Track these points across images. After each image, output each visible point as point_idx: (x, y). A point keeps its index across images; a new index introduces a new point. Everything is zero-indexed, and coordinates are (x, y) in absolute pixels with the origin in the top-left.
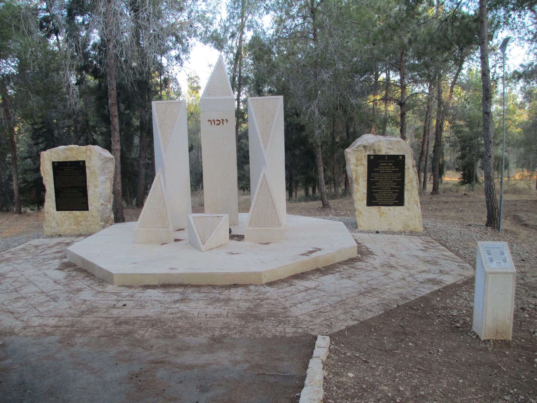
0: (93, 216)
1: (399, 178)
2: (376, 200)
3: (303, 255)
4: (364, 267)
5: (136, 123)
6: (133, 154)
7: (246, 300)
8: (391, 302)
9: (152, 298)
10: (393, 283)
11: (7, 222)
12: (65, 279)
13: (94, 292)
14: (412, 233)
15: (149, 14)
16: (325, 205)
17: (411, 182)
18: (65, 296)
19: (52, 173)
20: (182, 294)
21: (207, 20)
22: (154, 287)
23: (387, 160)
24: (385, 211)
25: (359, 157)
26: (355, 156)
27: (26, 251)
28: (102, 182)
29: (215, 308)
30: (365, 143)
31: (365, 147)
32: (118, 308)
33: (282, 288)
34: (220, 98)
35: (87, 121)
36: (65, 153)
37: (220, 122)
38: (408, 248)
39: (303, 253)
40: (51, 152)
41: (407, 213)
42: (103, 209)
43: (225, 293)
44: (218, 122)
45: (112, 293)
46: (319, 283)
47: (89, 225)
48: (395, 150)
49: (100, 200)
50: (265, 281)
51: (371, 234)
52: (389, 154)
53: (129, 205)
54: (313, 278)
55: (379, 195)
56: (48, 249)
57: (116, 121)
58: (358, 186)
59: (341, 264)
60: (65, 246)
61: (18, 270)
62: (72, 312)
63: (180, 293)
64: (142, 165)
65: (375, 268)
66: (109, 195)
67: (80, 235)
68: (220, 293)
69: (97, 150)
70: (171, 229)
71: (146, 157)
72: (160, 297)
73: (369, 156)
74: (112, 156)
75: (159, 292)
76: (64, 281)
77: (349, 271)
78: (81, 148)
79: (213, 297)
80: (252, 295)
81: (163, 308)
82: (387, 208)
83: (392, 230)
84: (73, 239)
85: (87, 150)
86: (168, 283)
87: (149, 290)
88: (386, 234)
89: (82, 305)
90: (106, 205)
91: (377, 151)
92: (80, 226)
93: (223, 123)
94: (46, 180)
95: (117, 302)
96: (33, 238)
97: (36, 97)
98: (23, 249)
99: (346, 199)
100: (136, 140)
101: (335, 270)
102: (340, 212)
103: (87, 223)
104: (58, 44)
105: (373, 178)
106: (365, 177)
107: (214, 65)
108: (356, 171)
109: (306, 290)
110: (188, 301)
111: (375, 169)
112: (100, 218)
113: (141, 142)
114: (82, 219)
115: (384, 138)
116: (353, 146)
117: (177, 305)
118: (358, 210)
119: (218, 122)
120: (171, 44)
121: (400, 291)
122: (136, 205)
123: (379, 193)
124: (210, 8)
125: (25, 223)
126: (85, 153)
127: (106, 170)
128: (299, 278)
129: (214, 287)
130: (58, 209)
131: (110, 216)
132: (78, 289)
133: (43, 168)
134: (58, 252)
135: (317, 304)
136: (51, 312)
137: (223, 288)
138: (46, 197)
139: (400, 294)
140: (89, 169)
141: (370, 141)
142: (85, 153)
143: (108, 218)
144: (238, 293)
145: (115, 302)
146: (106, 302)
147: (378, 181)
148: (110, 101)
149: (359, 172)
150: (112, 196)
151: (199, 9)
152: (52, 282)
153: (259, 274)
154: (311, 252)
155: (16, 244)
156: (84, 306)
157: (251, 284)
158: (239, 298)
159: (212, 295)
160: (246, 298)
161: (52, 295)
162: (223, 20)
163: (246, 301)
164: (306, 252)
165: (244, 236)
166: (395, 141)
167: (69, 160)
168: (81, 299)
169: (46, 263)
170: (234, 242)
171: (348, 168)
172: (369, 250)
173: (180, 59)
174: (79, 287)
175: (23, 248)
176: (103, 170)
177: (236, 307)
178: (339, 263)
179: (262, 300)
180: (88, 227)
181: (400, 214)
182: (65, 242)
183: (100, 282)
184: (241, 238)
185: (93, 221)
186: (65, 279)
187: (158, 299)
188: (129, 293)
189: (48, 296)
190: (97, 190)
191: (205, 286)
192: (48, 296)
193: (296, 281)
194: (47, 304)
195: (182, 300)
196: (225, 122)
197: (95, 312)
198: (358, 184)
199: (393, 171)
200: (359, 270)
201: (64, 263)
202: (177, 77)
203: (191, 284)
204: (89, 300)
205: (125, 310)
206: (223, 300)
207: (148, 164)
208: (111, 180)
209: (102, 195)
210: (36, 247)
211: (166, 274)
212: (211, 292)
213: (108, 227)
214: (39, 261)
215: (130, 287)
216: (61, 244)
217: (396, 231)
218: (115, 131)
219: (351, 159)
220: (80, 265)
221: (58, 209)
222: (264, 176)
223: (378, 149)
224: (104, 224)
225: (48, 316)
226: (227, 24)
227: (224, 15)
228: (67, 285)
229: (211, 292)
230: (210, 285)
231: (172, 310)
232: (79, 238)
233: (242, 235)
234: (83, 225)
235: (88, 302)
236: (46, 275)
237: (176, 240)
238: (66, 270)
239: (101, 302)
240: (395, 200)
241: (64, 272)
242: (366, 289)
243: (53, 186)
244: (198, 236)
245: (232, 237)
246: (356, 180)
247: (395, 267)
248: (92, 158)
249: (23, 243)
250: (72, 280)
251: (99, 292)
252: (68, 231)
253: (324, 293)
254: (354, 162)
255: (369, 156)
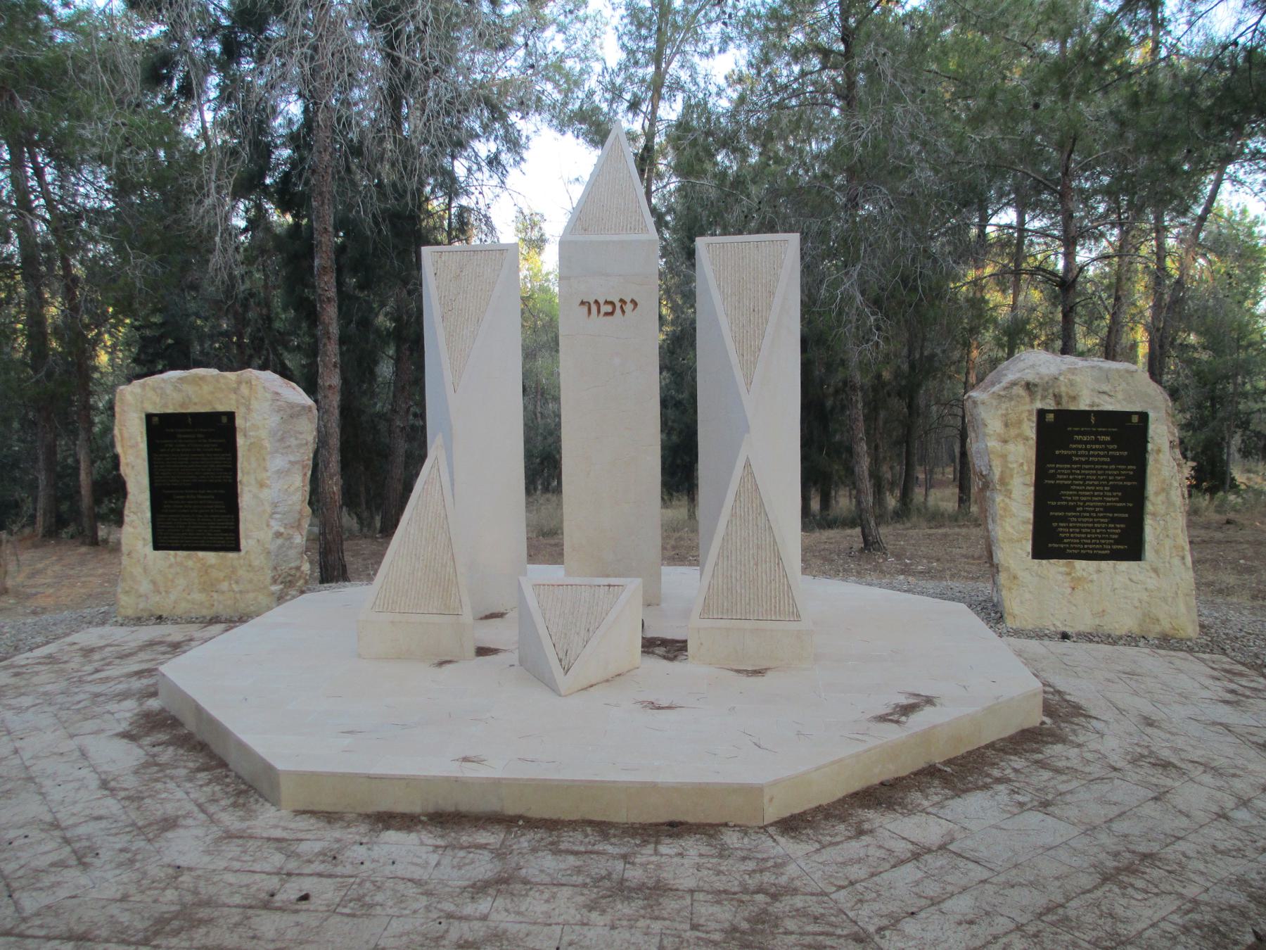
0: (250, 566)
1: (1128, 478)
2: (1060, 540)
3: (883, 719)
4: (1075, 763)
5: (383, 321)
6: (379, 405)
7: (720, 892)
8: (1227, 916)
9: (400, 870)
10: (1196, 831)
11: (57, 568)
12: (136, 772)
13: (216, 831)
14: (1167, 642)
15: (422, 27)
16: (870, 545)
17: (1165, 490)
18: (118, 846)
19: (143, 446)
20: (500, 854)
21: (567, 76)
22: (407, 822)
23: (1096, 425)
24: (1085, 574)
25: (1013, 417)
26: (1000, 412)
27: (56, 667)
28: (279, 472)
29: (613, 928)
30: (1030, 376)
31: (1029, 386)
32: (281, 909)
33: (832, 844)
34: (615, 238)
35: (269, 319)
36: (180, 391)
37: (614, 308)
38: (1180, 694)
39: (882, 711)
40: (143, 386)
41: (1152, 582)
42: (281, 547)
43: (644, 859)
44: (609, 308)
45: (269, 839)
46: (951, 825)
47: (241, 592)
48: (1120, 396)
49: (273, 523)
50: (772, 813)
51: (1046, 642)
52: (1100, 408)
53: (365, 530)
54: (926, 803)
55: (1069, 527)
56: (118, 661)
57: (331, 313)
58: (1007, 500)
59: (1003, 750)
60: (164, 653)
61: (9, 733)
62: (125, 918)
63: (492, 851)
64: (398, 430)
65: (1115, 769)
66: (298, 507)
67: (214, 620)
68: (624, 857)
69: (267, 384)
70: (468, 616)
71: (408, 409)
72: (425, 865)
73: (1041, 413)
74: (309, 401)
75: (422, 844)
76: (131, 782)
77: (1034, 780)
78: (225, 377)
79: (604, 873)
80: (736, 874)
81: (434, 915)
82: (1091, 565)
83: (1107, 629)
84: (194, 631)
85: (239, 383)
86: (453, 809)
87: (391, 836)
88: (1091, 641)
89: (164, 889)
90: (290, 538)
91: (1065, 400)
92: (215, 595)
93: (623, 312)
94: (127, 464)
95: (283, 882)
96: (90, 623)
97: (143, 257)
98: (51, 659)
99: (908, 525)
100: (386, 370)
101: (988, 775)
102: (911, 564)
103: (235, 587)
104: (204, 133)
105: (1053, 477)
106: (1028, 473)
107: (586, 178)
108: (1004, 457)
109: (916, 856)
110: (519, 886)
111: (1057, 452)
112: (269, 574)
113: (397, 373)
114: (221, 575)
115: (1085, 363)
116: (993, 384)
117: (484, 905)
118: (1008, 569)
119: (609, 308)
120: (477, 126)
121: (1235, 867)
122: (381, 532)
123: (1069, 522)
124: (574, 47)
125: (100, 571)
126: (235, 391)
127: (292, 440)
128: (880, 804)
129: (603, 828)
130: (157, 546)
131: (298, 568)
132: (166, 820)
133: (121, 430)
134: (139, 674)
135: (971, 922)
136: (57, 915)
137: (633, 836)
138: (126, 512)
139: (1241, 882)
140: (245, 436)
141: (1044, 371)
142: (235, 391)
143: (293, 572)
144: (685, 861)
145: (274, 882)
146: (245, 879)
147: (1067, 487)
148: (317, 262)
149: (1011, 458)
150: (308, 510)
151: (549, 50)
152: (94, 783)
153: (752, 792)
154: (907, 710)
155: (39, 639)
156: (170, 894)
157: (726, 825)
158: (690, 883)
159: (599, 867)
160: (719, 886)
161: (80, 839)
162: (610, 70)
163: (720, 895)
164: (889, 710)
165: (685, 642)
166: (1118, 371)
167: (189, 411)
168: (166, 860)
169: (97, 710)
170: (656, 665)
171: (974, 446)
172: (1068, 697)
173: (499, 163)
174: (170, 809)
175: (50, 656)
176: (282, 439)
177: (687, 927)
178: (992, 746)
179: (775, 897)
180: (238, 596)
181: (1129, 582)
182: (169, 639)
183: (240, 793)
184: (673, 649)
185: (251, 581)
186: (136, 772)
187: (418, 873)
188: (326, 844)
189: (67, 841)
190: (266, 494)
191: (574, 825)
192: (67, 841)
193: (873, 817)
194: (53, 879)
195: (501, 883)
196: (629, 307)
197: (201, 922)
198: (1008, 494)
199: (1112, 457)
200: (1064, 778)
201: (147, 715)
202: (491, 213)
203: (529, 814)
204: (190, 869)
205: (302, 918)
206: (641, 888)
207: (413, 427)
208: (304, 467)
209: (279, 509)
210: (88, 652)
211: (447, 779)
212: (597, 853)
213: (294, 597)
214: (79, 702)
215: (330, 817)
216: (155, 647)
217: (1118, 633)
218: (329, 338)
219: (988, 421)
220: (191, 725)
221: (157, 546)
222: (748, 464)
223: (1067, 394)
224: (282, 590)
225: (43, 933)
226: (618, 81)
227: (613, 55)
228: (135, 798)
229: (597, 853)
230: (590, 823)
231: (465, 925)
232: (210, 628)
233: (678, 641)
234: (223, 592)
235: (186, 878)
236: (84, 754)
237: (482, 651)
238: (147, 741)
239: (230, 878)
240: (1117, 542)
241: (141, 747)
242: (1116, 855)
243: (145, 481)
244: (547, 644)
245: (650, 645)
246: (1003, 481)
247: (1175, 767)
248: (255, 405)
249: (57, 638)
250: (157, 780)
251: (230, 836)
252: (183, 607)
253: (978, 873)
254: (998, 431)
255: (1041, 413)
